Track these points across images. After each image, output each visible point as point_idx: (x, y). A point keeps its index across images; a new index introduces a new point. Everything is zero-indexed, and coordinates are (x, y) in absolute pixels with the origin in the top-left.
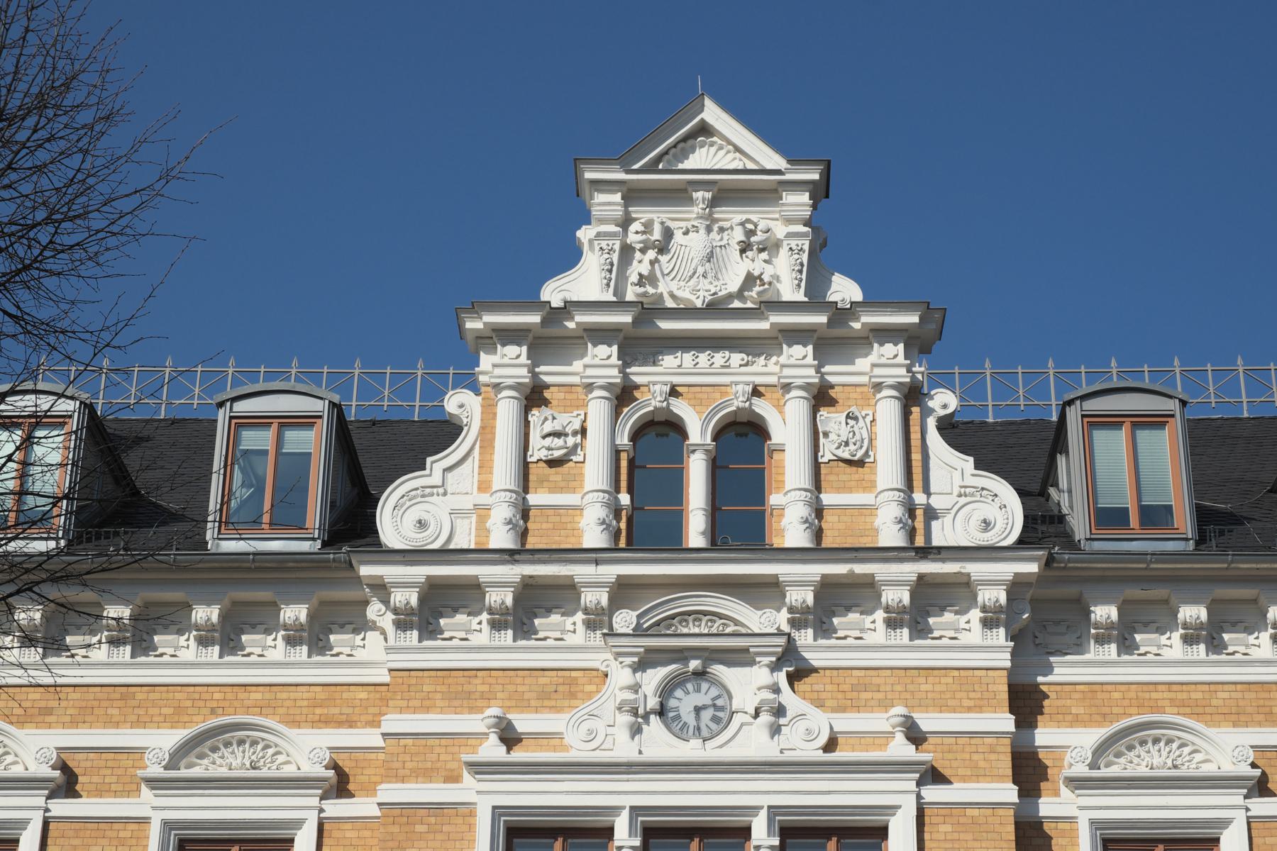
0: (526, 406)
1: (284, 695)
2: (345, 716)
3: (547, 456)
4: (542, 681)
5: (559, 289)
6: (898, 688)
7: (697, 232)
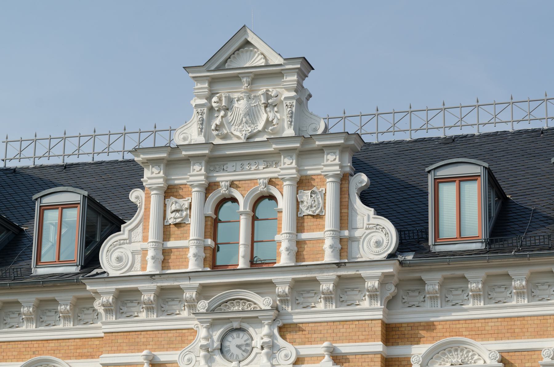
0: (165, 196)
1: (64, 344)
2: (90, 353)
3: (173, 222)
4: (170, 335)
5: (181, 133)
6: (330, 331)
7: (243, 99)
